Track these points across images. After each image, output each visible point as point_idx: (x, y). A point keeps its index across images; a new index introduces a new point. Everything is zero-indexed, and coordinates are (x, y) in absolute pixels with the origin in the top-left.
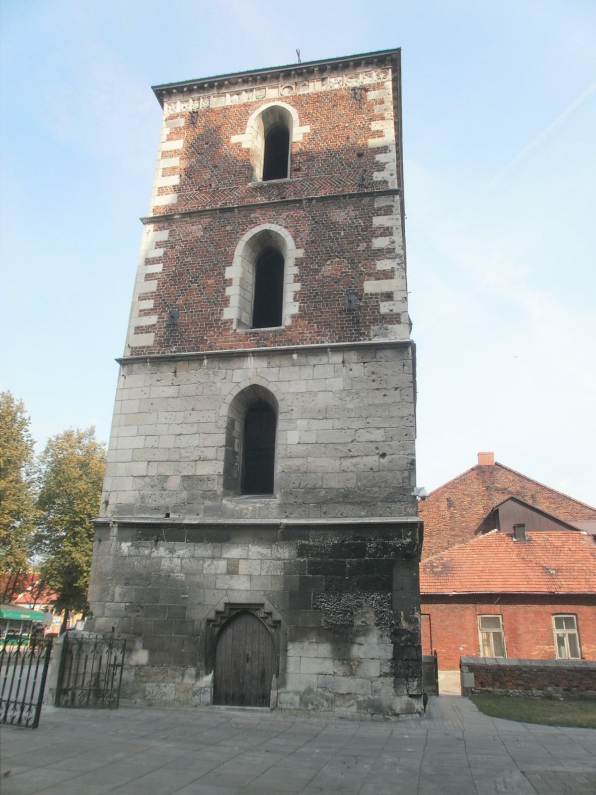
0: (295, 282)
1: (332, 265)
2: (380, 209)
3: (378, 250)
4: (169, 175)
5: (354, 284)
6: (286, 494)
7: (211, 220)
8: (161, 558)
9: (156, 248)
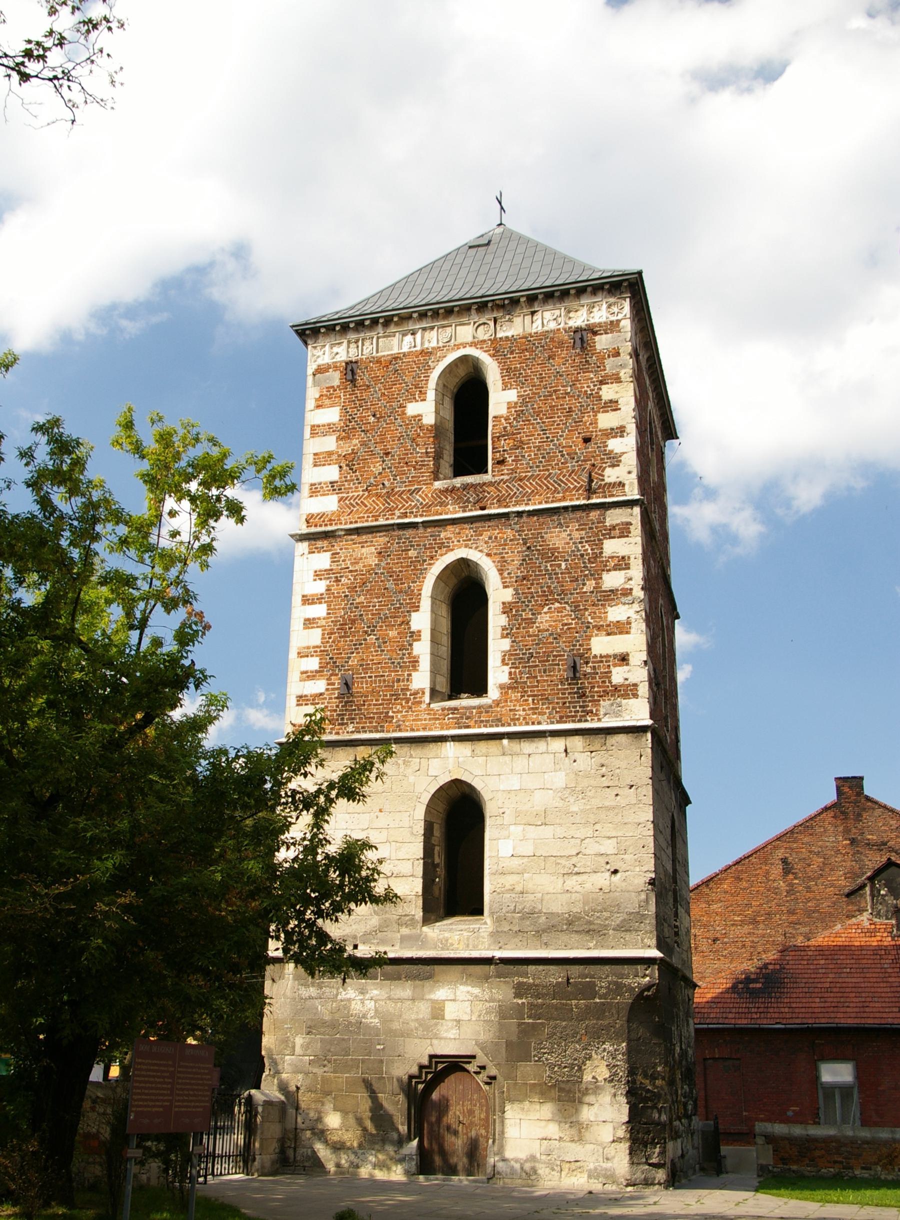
0: (503, 637)
1: (551, 613)
2: (613, 528)
3: (610, 591)
4: (324, 465)
5: (578, 641)
6: (498, 921)
7: (387, 539)
8: (349, 1000)
9: (315, 580)
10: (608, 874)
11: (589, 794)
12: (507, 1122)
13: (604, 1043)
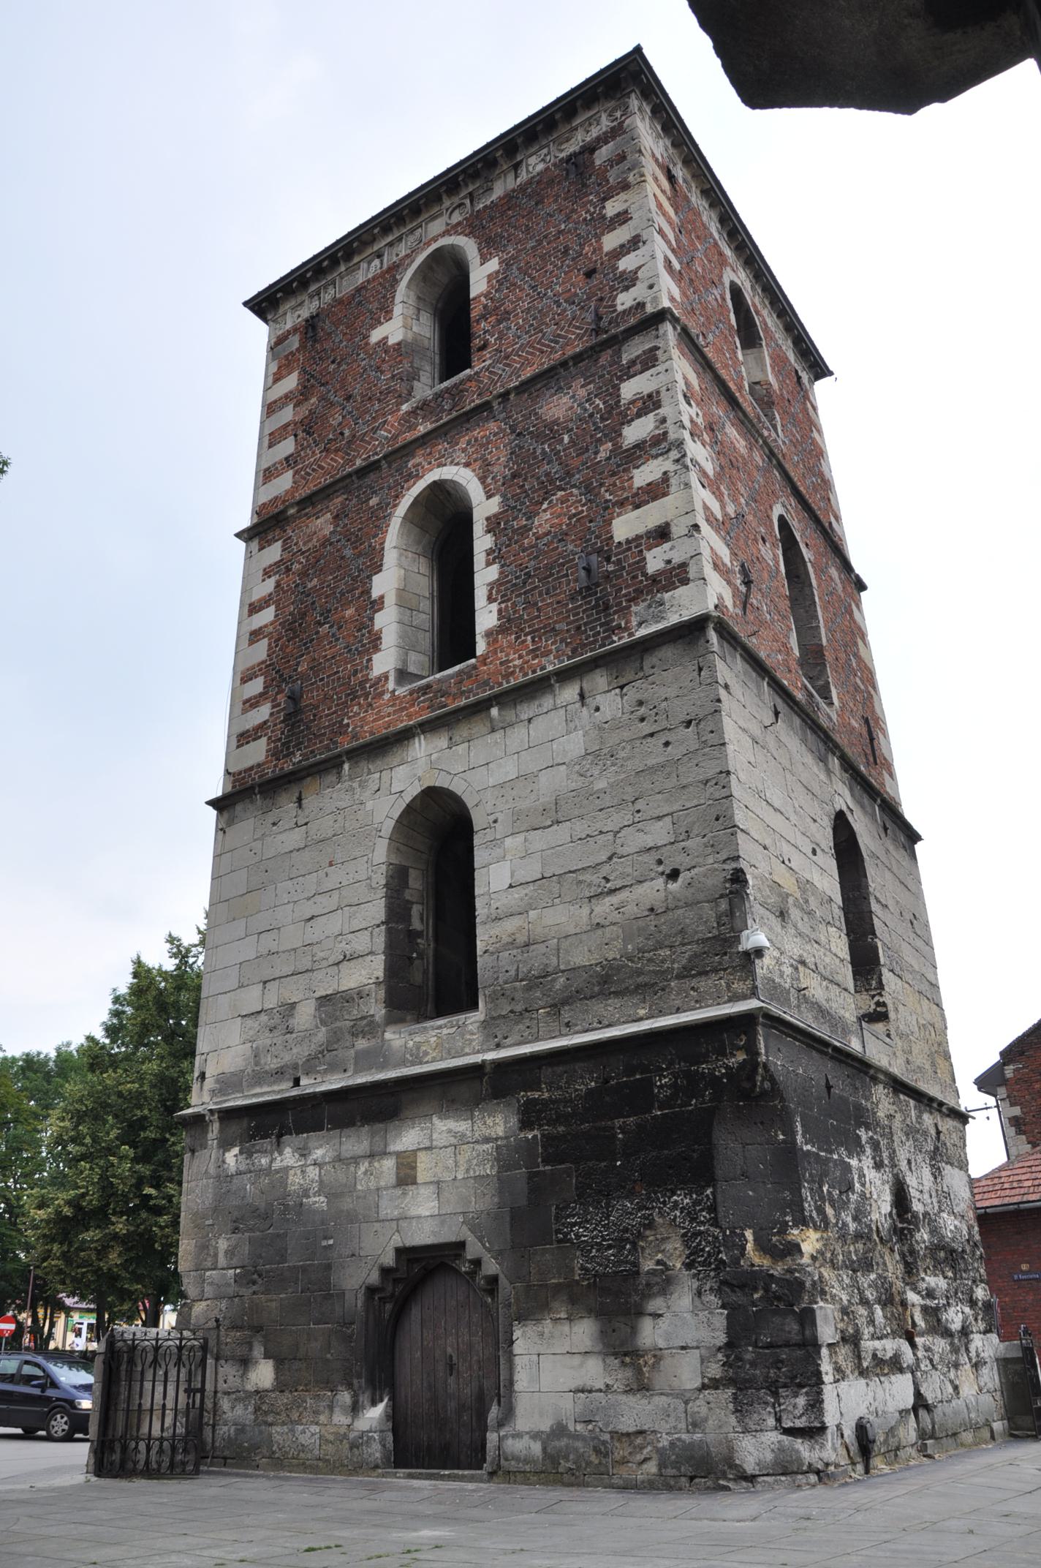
2: (633, 363)
10: (661, 880)
11: (622, 754)
12: (517, 1360)
13: (674, 1194)
